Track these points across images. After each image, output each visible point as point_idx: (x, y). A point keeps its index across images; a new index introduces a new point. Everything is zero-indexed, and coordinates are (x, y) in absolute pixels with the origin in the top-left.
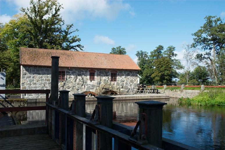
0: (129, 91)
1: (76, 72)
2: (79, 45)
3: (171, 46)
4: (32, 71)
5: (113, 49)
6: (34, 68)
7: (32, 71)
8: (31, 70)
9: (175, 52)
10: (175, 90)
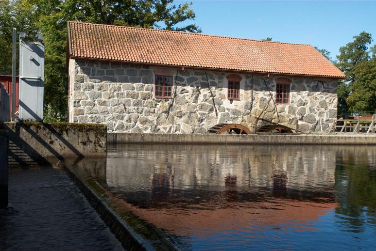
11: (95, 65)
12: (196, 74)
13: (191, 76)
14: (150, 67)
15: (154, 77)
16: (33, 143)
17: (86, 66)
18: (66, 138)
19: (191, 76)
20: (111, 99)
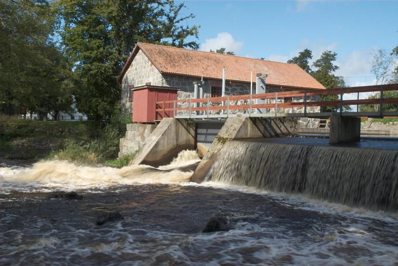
0: (309, 124)
1: (236, 90)
2: (194, 43)
3: (329, 50)
4: (175, 84)
5: (307, 49)
6: (178, 80)
7: (175, 84)
8: (173, 83)
9: (334, 63)
10: (391, 123)
11: (174, 79)
12: (237, 86)
13: (233, 87)
14: (208, 80)
15: (210, 88)
16: (275, 127)
17: (169, 79)
18: (285, 125)
19: (233, 87)
20: (184, 103)
